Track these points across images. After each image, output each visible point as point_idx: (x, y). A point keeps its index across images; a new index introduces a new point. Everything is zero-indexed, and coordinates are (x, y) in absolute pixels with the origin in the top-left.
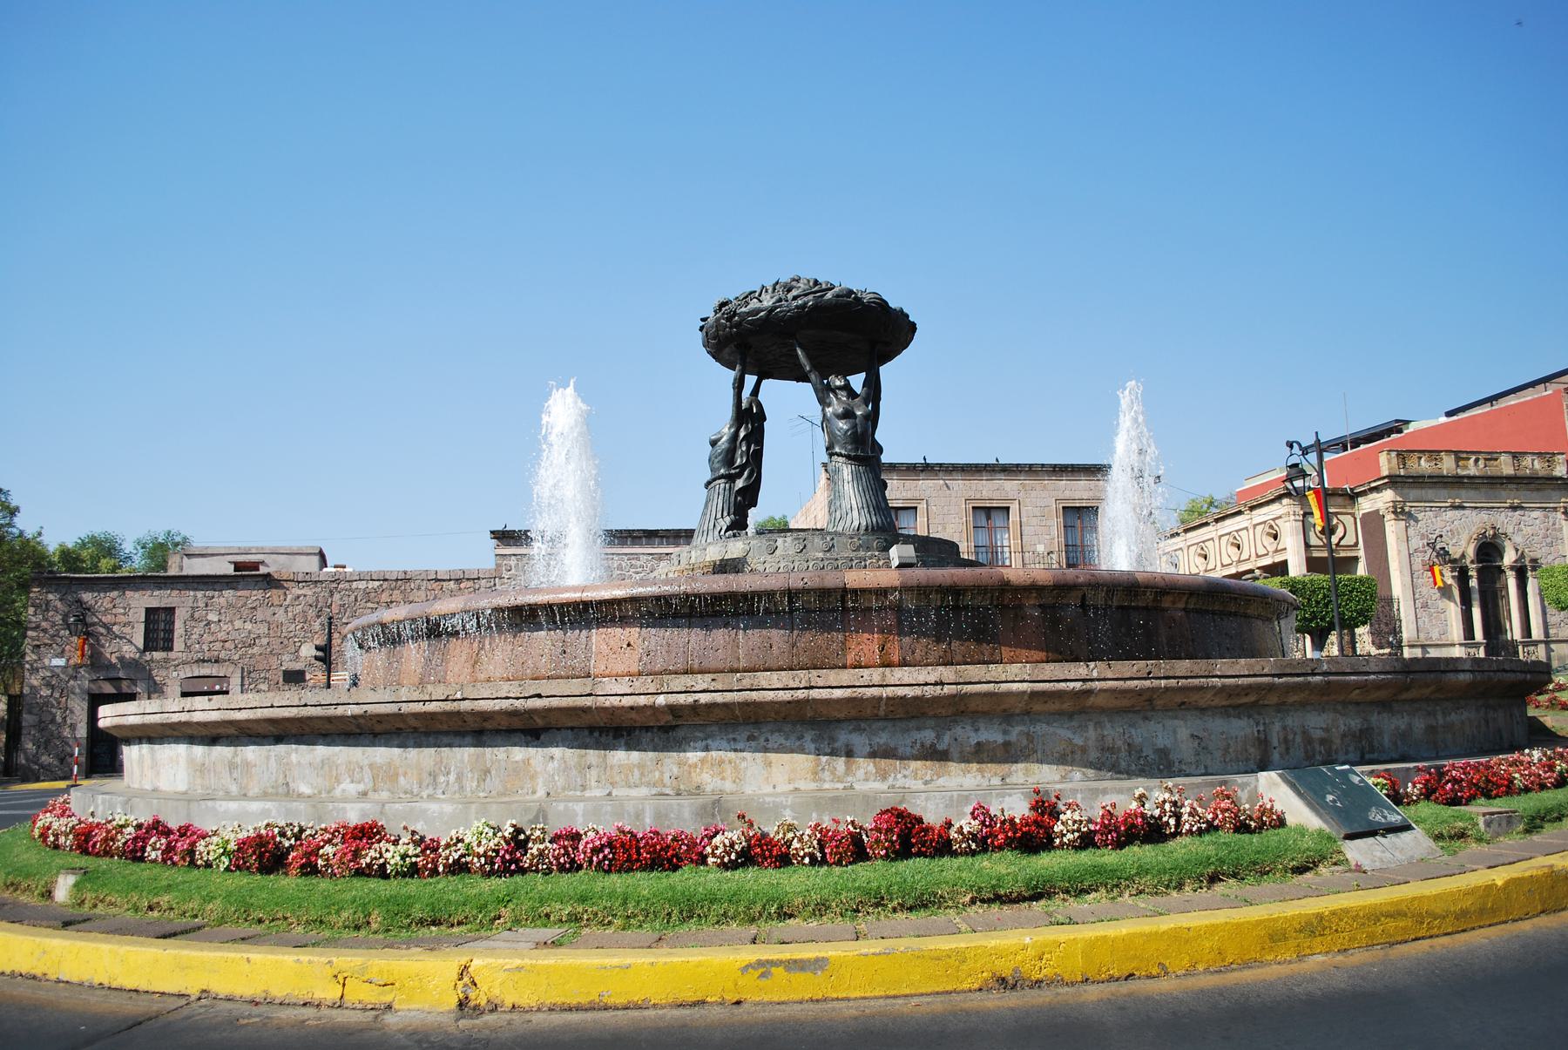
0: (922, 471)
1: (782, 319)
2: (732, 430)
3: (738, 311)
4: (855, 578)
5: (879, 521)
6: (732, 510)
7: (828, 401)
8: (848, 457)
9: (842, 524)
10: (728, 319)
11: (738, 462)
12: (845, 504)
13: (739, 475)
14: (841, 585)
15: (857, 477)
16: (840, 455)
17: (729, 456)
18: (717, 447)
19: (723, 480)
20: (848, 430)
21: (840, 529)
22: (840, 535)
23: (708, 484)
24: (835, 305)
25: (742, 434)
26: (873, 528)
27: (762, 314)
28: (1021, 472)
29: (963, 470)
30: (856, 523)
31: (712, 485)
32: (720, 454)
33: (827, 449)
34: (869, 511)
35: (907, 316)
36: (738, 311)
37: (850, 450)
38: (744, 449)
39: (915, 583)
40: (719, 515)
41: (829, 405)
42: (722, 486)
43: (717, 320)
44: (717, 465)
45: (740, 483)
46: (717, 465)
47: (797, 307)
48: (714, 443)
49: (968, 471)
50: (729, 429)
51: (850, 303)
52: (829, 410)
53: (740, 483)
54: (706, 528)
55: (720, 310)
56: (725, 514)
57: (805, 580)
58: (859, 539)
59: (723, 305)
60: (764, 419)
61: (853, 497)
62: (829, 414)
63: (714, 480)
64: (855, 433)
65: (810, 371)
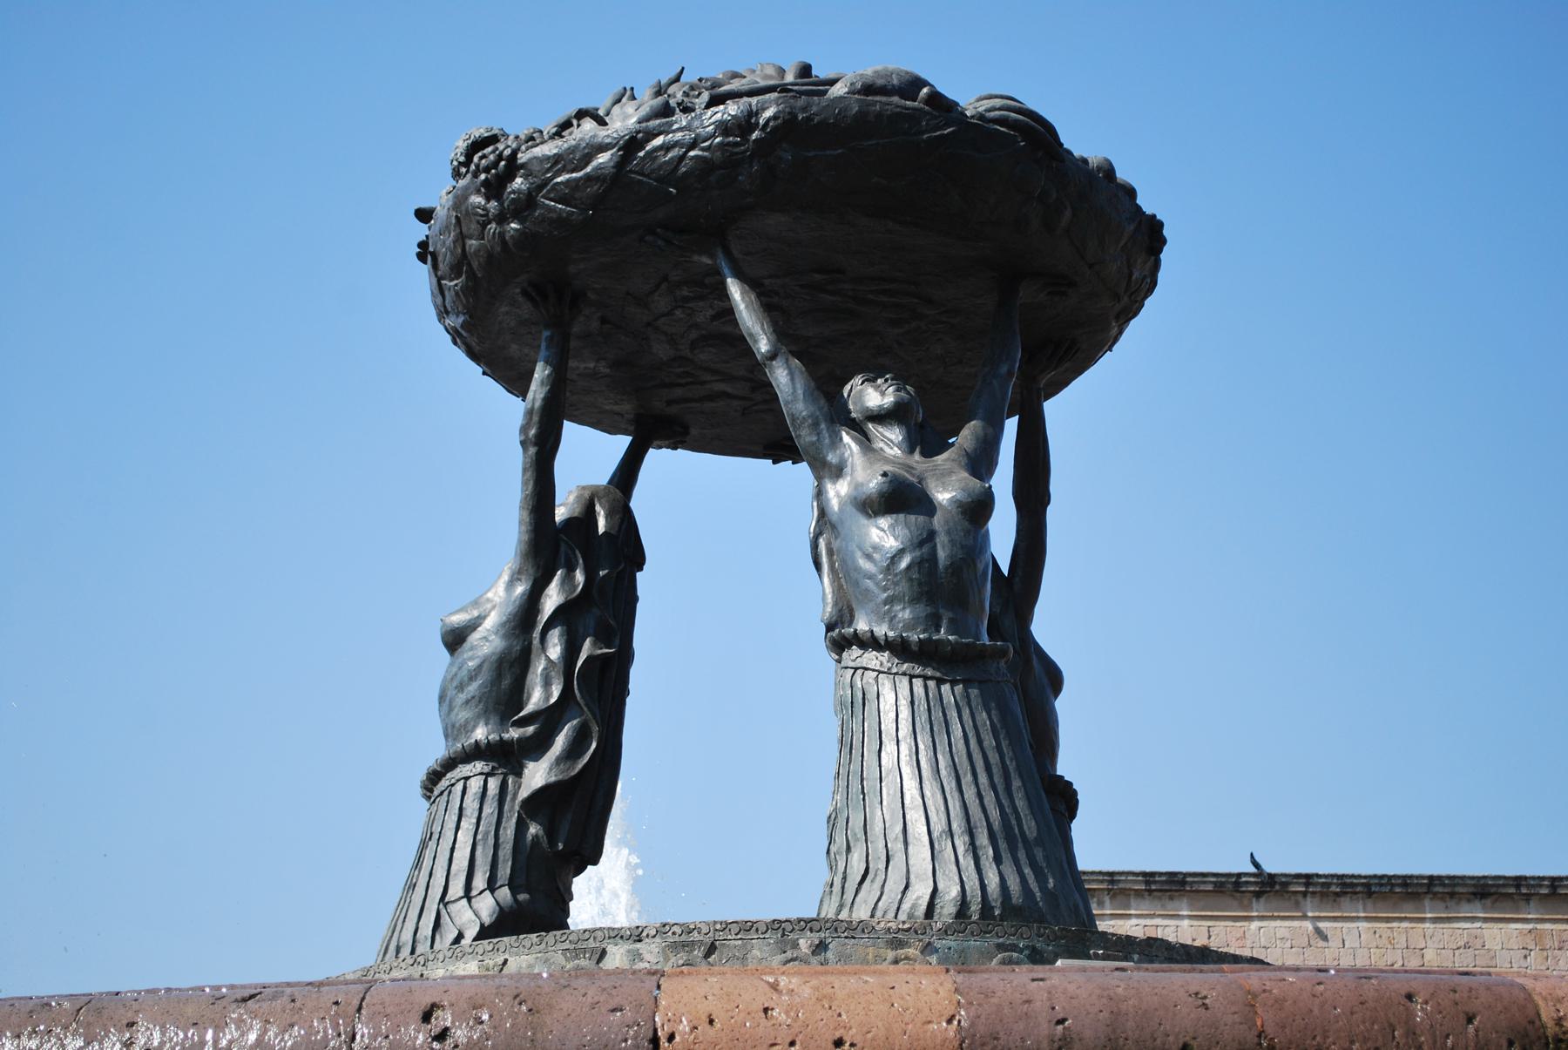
0: (1258, 895)
1: (670, 174)
2: (520, 589)
3: (522, 158)
4: (713, 1006)
6: (505, 871)
8: (899, 649)
9: (870, 892)
10: (494, 188)
12: (884, 815)
13: (536, 747)
15: (933, 721)
16: (870, 643)
17: (506, 683)
19: (479, 766)
20: (900, 553)
21: (862, 913)
23: (434, 777)
24: (862, 115)
25: (552, 599)
27: (603, 158)
28: (1528, 898)
29: (1370, 894)
30: (921, 892)
31: (444, 783)
33: (830, 628)
34: (973, 848)
35: (1131, 192)
36: (522, 158)
37: (909, 626)
38: (555, 651)
40: (457, 889)
41: (838, 472)
42: (475, 785)
43: (460, 201)
44: (462, 715)
45: (537, 774)
46: (462, 715)
47: (724, 128)
48: (455, 639)
49: (1383, 896)
50: (511, 584)
51: (913, 116)
52: (838, 492)
53: (537, 774)
54: (407, 936)
55: (467, 164)
56: (480, 882)
57: (444, 1018)
59: (477, 146)
60: (637, 558)
61: (911, 786)
62: (834, 504)
63: (450, 764)
64: (929, 564)
65: (773, 356)
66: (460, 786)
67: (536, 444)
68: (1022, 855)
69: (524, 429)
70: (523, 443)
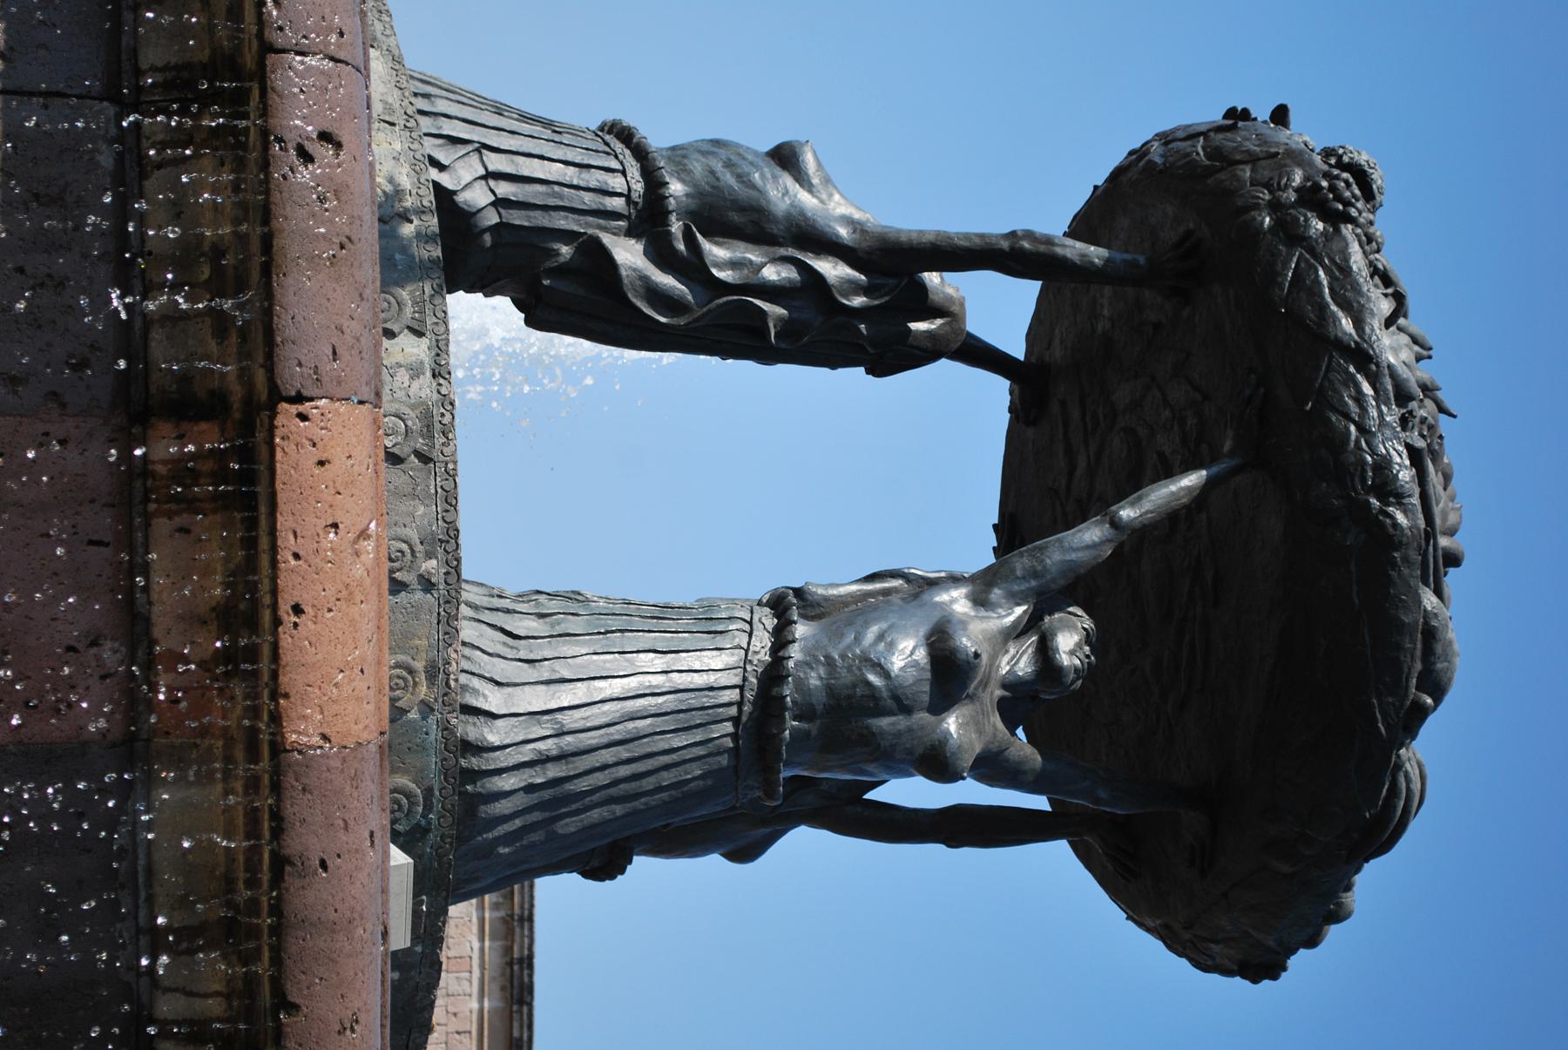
2: (843, 232)
3: (1347, 230)
4: (339, 465)
5: (503, 807)
6: (517, 218)
7: (996, 594)
8: (774, 673)
9: (493, 641)
11: (716, 252)
12: (580, 656)
13: (661, 254)
14: (292, 376)
16: (781, 640)
17: (735, 217)
18: (770, 169)
19: (638, 187)
20: (885, 673)
21: (468, 631)
22: (448, 622)
23: (624, 134)
24: (1400, 627)
25: (832, 270)
26: (475, 762)
27: (1347, 324)
31: (619, 147)
32: (741, 177)
33: (798, 592)
34: (543, 761)
36: (1347, 230)
37: (800, 685)
38: (771, 273)
39: (305, 841)
40: (496, 163)
41: (980, 601)
42: (617, 183)
43: (1297, 157)
44: (697, 167)
45: (629, 254)
46: (697, 167)
47: (1383, 465)
48: (785, 157)
51: (1399, 687)
52: (957, 601)
53: (629, 254)
54: (442, 106)
56: (504, 189)
58: (426, 708)
59: (1362, 177)
60: (879, 369)
62: (943, 597)
64: (872, 703)
65: (1115, 524)
66: (615, 164)
67: (1012, 248)
68: (536, 816)
69: (1029, 235)
70: (1013, 234)
